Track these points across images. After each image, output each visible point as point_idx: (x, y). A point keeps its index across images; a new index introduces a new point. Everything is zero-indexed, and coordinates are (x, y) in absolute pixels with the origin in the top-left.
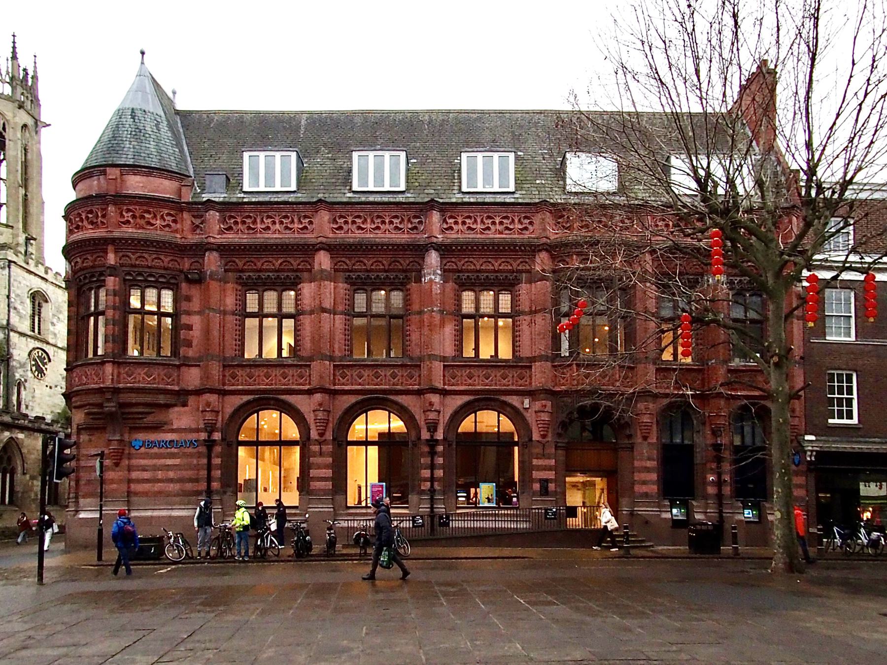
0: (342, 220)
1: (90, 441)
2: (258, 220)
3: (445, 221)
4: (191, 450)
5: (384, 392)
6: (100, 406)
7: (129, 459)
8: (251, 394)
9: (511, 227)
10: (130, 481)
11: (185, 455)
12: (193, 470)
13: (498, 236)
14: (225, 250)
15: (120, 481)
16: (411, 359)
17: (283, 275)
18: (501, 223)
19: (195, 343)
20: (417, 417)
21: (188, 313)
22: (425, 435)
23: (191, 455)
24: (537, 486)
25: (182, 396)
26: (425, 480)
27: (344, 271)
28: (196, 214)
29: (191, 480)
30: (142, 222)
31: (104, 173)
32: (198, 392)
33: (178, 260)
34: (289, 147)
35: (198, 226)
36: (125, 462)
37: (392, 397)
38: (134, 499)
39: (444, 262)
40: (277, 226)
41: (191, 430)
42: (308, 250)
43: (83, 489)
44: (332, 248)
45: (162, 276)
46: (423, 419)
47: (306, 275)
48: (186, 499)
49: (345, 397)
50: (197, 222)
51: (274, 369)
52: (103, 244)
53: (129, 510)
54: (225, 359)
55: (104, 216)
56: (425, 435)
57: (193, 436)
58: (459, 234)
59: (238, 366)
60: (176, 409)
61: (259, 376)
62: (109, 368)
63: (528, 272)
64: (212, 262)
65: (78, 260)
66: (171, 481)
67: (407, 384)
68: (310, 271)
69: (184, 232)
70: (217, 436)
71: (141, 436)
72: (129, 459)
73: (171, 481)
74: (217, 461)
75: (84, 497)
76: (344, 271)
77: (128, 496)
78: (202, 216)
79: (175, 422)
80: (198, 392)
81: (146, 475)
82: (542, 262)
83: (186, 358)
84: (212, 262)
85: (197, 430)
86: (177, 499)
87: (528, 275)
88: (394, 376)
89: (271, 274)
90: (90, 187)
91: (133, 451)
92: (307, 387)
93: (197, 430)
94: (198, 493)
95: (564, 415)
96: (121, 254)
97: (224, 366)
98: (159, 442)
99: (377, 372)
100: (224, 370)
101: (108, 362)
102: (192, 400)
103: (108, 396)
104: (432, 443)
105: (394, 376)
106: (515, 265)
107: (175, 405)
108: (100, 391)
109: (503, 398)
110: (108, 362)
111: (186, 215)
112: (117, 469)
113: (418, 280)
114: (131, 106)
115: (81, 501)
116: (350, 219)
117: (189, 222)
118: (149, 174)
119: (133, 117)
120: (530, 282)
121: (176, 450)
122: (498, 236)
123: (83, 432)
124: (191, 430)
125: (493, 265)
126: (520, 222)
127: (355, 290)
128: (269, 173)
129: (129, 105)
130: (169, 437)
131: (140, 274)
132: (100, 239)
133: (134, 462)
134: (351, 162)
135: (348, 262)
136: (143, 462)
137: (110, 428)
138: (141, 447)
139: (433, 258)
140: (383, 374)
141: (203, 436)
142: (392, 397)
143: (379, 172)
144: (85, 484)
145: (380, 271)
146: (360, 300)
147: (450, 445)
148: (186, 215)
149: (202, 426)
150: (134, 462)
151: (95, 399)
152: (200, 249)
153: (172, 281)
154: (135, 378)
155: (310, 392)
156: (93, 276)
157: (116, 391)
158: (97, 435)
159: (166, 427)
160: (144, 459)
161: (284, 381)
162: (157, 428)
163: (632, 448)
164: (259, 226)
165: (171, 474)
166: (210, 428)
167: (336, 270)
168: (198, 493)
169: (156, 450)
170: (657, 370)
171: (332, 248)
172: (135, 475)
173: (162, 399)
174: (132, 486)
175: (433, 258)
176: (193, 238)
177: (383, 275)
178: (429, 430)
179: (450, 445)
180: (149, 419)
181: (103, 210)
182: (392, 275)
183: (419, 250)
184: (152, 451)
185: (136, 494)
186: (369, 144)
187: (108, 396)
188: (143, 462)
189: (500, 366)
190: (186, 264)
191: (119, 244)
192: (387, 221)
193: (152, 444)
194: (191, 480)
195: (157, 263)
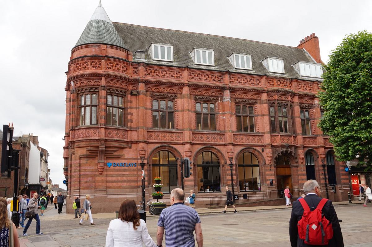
0: (193, 75)
1: (87, 163)
2: (161, 72)
3: (230, 79)
4: (133, 168)
5: (212, 144)
6: (98, 147)
7: (106, 171)
8: (204, 145)
9: (273, 84)
10: (107, 182)
11: (130, 170)
12: (135, 177)
13: (249, 86)
14: (147, 83)
15: (103, 182)
16: (178, 129)
17: (170, 95)
18: (198, 76)
19: (134, 121)
20: (225, 155)
21: (131, 108)
22: (228, 162)
23: (134, 170)
24: (268, 182)
25: (129, 144)
26: (229, 180)
27: (194, 95)
28: (135, 67)
29: (134, 181)
30: (198, 78)
31: (99, 47)
32: (137, 143)
33: (159, 88)
34: (170, 43)
35: (135, 72)
36: (105, 173)
37: (214, 147)
38: (109, 190)
39: (191, 91)
40: (168, 75)
41: (134, 159)
42: (181, 86)
43: (83, 185)
44: (190, 86)
45: (121, 92)
46: (227, 156)
47: (179, 95)
48: (132, 190)
49: (197, 146)
50: (135, 70)
51: (160, 133)
52: (100, 76)
53: (80, 196)
54: (147, 129)
55: (100, 64)
56: (228, 162)
57: (135, 162)
58: (196, 81)
59: (153, 132)
60: (126, 149)
61: (161, 136)
62: (103, 130)
63: (260, 100)
64: (141, 87)
65: (78, 83)
66: (125, 181)
67: (219, 142)
68: (181, 94)
69: (130, 74)
70: (145, 162)
71: (111, 161)
72: (106, 171)
73: (125, 181)
74: (234, 172)
75: (84, 189)
76: (194, 95)
77: (106, 189)
78: (137, 68)
79: (126, 155)
80: (137, 143)
81: (114, 179)
82: (264, 96)
83: (131, 127)
84: (141, 87)
85: (137, 159)
86: (128, 190)
87: (259, 101)
88: (214, 138)
89: (157, 93)
90: (91, 51)
91: (108, 168)
92: (181, 142)
93: (137, 159)
94: (138, 187)
95: (277, 154)
96: (300, 99)
97: (147, 131)
98: (119, 164)
99: (195, 136)
100: (147, 133)
101: (103, 127)
102: (134, 146)
103: (103, 142)
104: (231, 165)
105: (248, 139)
106: (249, 96)
107: (126, 148)
108: (99, 140)
109: (255, 148)
110: (103, 127)
111: (131, 66)
112: (101, 176)
113: (222, 100)
114: (95, 19)
115: (81, 191)
116: (196, 75)
117: (132, 70)
118: (117, 49)
119: (104, 24)
120: (260, 103)
121: (127, 168)
122: (249, 86)
123: (82, 158)
124: (134, 159)
125: (195, 92)
126: (204, 76)
127: (197, 103)
128: (163, 53)
129: (94, 19)
130: (123, 162)
131: (113, 90)
132: (99, 74)
133: (109, 173)
134: (214, 55)
135: (196, 91)
136: (112, 173)
137: (98, 158)
138: (111, 166)
139: (227, 92)
140: (210, 137)
141: (140, 162)
142: (214, 147)
143: (203, 58)
144: (85, 183)
145: (172, 93)
146: (155, 104)
147: (150, 166)
148: (131, 66)
149: (139, 157)
150: (109, 173)
151: (96, 144)
152: (137, 82)
153: (124, 94)
154: (112, 135)
155: (225, 145)
156: (82, 90)
157: (106, 140)
158: (91, 160)
159: (122, 157)
160: (112, 171)
161: (95, 135)
162: (118, 157)
163: (297, 167)
164: (161, 74)
165: (125, 179)
166: (142, 158)
167: (191, 95)
168: (138, 187)
169: (118, 168)
170: (192, 133)
171: (190, 86)
172: (109, 179)
173: (122, 145)
174: (108, 184)
175: (227, 92)
176: (134, 77)
177: (307, 105)
178: (230, 160)
179: (150, 166)
180: (116, 153)
181: (99, 62)
182: (212, 98)
183: (222, 89)
184: (116, 168)
185: (109, 187)
186: (238, 51)
187: (103, 142)
188: (112, 173)
189: (252, 135)
190: (130, 87)
191: (107, 76)
192: (153, 71)
193: (115, 165)
194: (134, 181)
195: (171, 91)
